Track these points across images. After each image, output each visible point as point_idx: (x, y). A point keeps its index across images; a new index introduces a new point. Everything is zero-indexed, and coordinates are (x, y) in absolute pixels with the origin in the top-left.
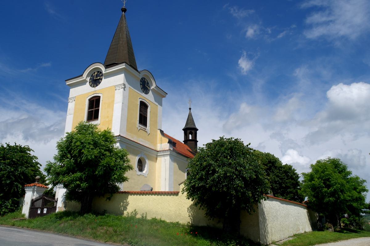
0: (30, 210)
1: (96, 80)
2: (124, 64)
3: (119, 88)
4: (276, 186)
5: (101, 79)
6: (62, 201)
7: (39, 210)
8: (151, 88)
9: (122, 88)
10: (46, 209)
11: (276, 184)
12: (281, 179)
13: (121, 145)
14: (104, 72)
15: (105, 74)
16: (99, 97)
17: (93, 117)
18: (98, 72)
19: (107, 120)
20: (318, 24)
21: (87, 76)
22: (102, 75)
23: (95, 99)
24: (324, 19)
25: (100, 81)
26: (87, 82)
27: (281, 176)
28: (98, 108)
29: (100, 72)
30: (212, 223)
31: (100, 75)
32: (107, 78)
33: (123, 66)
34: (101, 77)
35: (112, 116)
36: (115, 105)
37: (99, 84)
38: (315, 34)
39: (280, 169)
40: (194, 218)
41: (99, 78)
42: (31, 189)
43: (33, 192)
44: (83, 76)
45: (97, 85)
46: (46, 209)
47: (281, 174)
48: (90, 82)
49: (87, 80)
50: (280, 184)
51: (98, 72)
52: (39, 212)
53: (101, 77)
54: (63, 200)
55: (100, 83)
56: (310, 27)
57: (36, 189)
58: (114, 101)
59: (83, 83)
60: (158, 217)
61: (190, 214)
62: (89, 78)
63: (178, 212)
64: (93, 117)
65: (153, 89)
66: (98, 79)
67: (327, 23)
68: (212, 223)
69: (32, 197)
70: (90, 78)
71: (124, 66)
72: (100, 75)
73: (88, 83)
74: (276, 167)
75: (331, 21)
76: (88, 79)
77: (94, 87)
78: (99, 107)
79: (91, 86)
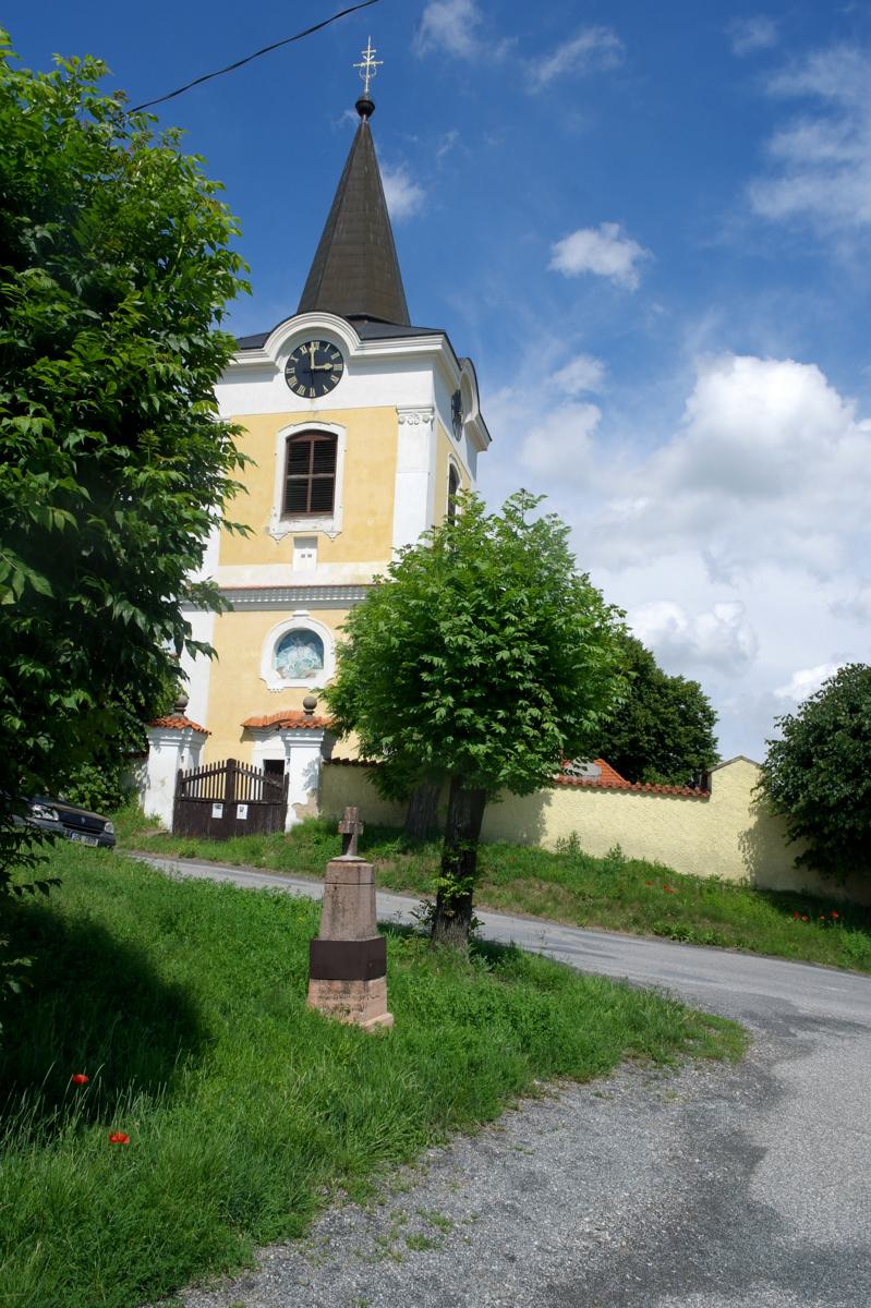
0: (176, 805)
1: (315, 371)
2: (440, 339)
3: (412, 420)
4: (649, 742)
5: (339, 374)
6: (306, 786)
7: (218, 808)
8: (467, 421)
9: (426, 422)
10: (246, 807)
11: (648, 735)
12: (666, 722)
13: (30, 529)
14: (353, 352)
15: (354, 358)
16: (333, 438)
17: (309, 502)
18: (323, 344)
19: (370, 523)
20: (806, 167)
21: (281, 352)
22: (340, 360)
23: (312, 439)
24: (828, 150)
25: (334, 378)
26: (277, 371)
27: (664, 713)
28: (330, 475)
29: (330, 348)
30: (809, 881)
31: (333, 357)
32: (365, 374)
33: (434, 345)
34: (337, 367)
35: (392, 513)
36: (397, 475)
37: (330, 390)
38: (778, 201)
39: (663, 690)
40: (759, 865)
41: (327, 366)
42: (175, 738)
43: (181, 749)
44: (267, 347)
45: (320, 393)
46: (246, 807)
47: (666, 708)
48: (288, 376)
49: (277, 364)
50: (660, 736)
51: (323, 344)
52: (217, 813)
53: (337, 367)
54: (309, 783)
55: (332, 386)
56: (778, 170)
57: (190, 739)
58: (393, 460)
59: (265, 372)
60: (650, 859)
61: (747, 857)
62: (286, 359)
63: (708, 850)
64: (309, 502)
65: (471, 422)
66: (323, 371)
67: (831, 169)
68: (809, 881)
69: (178, 764)
70: (290, 361)
71: (439, 347)
72: (333, 357)
73: (280, 377)
74: (649, 684)
75: (846, 164)
76: (282, 363)
77: (307, 395)
78: (333, 470)
79: (295, 389)
